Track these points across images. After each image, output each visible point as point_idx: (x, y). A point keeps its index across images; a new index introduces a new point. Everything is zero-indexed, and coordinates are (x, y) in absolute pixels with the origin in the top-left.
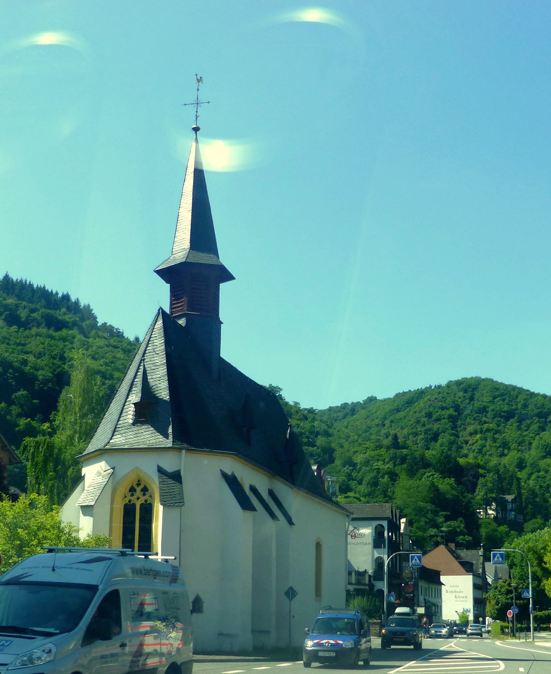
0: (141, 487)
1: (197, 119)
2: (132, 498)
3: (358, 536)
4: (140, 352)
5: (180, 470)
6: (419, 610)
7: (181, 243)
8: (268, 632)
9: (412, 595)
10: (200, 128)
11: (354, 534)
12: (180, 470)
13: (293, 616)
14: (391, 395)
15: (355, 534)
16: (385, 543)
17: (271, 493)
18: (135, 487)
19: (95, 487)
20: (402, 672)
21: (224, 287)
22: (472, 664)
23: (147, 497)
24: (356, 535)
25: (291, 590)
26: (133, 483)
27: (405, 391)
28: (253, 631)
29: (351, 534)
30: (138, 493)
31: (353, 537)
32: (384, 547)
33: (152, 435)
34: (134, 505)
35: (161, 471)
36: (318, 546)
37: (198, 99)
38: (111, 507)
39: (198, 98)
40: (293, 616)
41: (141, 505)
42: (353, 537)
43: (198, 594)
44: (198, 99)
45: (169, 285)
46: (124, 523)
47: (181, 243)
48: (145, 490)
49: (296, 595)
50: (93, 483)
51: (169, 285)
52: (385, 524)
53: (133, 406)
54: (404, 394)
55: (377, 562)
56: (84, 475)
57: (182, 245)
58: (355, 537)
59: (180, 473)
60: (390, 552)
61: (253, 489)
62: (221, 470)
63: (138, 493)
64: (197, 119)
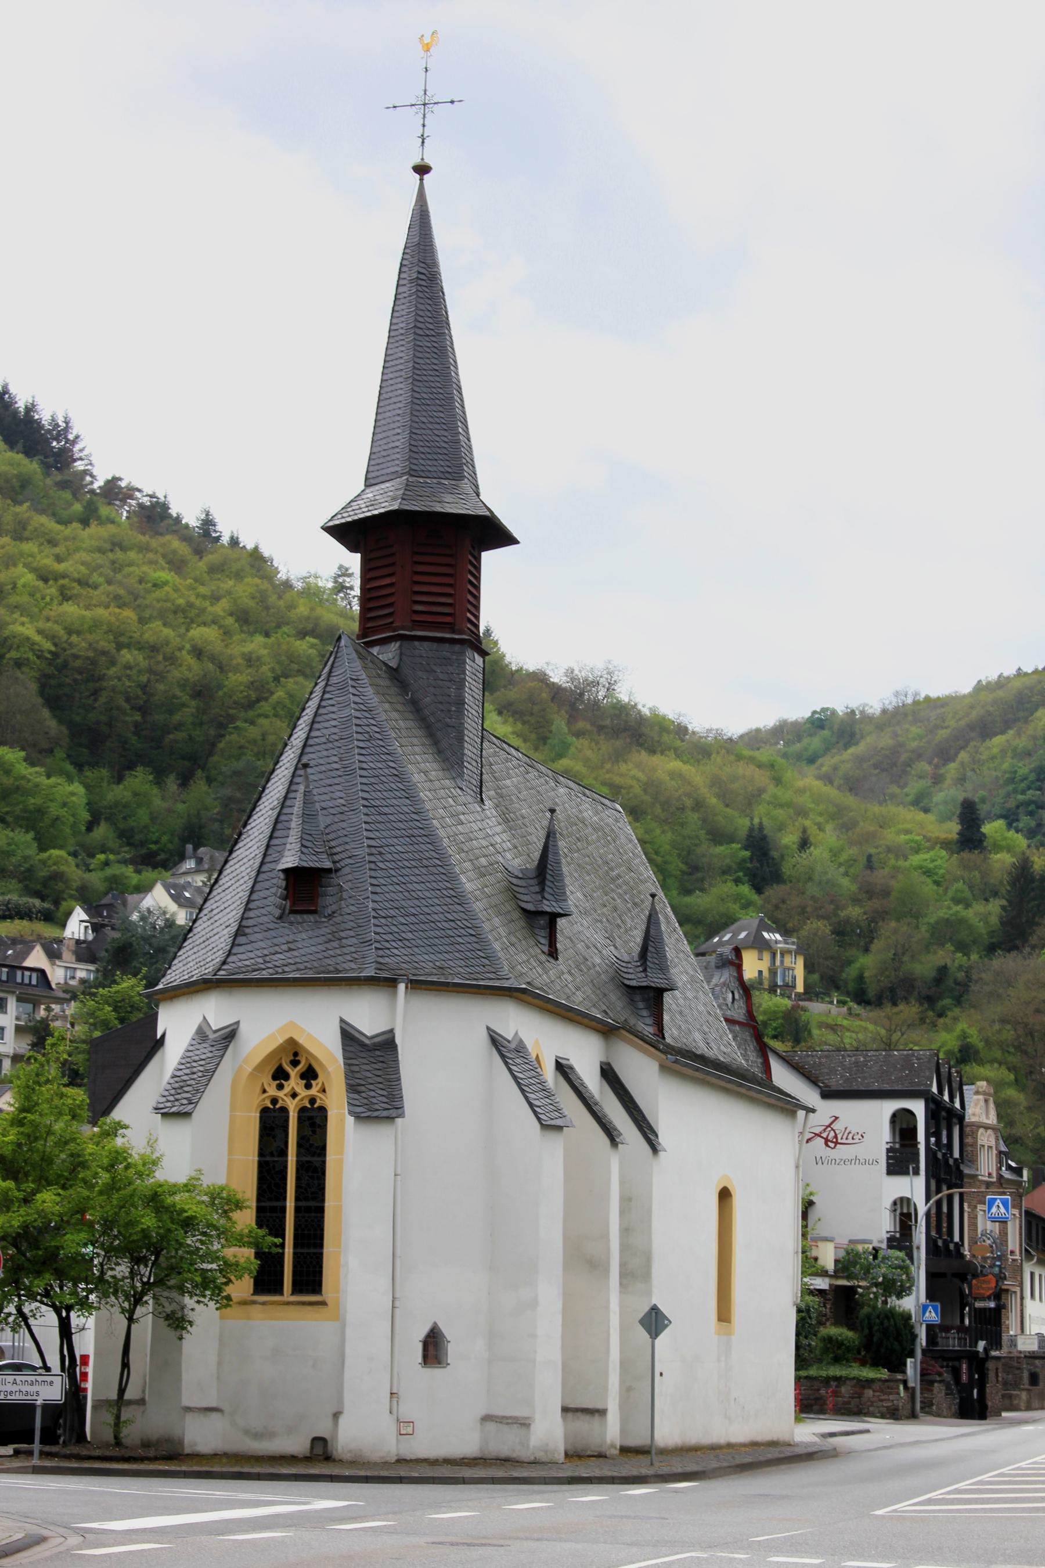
0: (301, 1067)
1: (423, 142)
2: (281, 1094)
3: (844, 1141)
4: (294, 743)
5: (391, 1031)
6: (1024, 1343)
7: (388, 459)
8: (602, 1412)
9: (992, 1305)
10: (432, 166)
11: (832, 1134)
12: (391, 1031)
13: (661, 1374)
14: (966, 688)
15: (836, 1137)
16: (918, 1162)
17: (608, 1074)
18: (288, 1068)
19: (195, 1070)
20: (903, 1512)
21: (491, 560)
22: (1016, 1498)
23: (314, 1091)
24: (839, 1137)
25: (654, 1314)
26: (14, 637)
27: (1005, 674)
28: (565, 1410)
29: (824, 1135)
30: (294, 1083)
31: (830, 1144)
32: (916, 1172)
33: (327, 945)
34: (284, 1110)
35: (349, 1036)
36: (725, 1195)
37: (424, 115)
38: (231, 1116)
39: (425, 91)
40: (661, 1374)
41: (302, 1110)
42: (830, 1144)
43: (435, 1323)
44: (424, 115)
45: (359, 555)
46: (261, 1153)
47: (388, 459)
48: (310, 1075)
49: (667, 1326)
50: (188, 1060)
51: (359, 555)
52: (918, 1108)
53: (282, 875)
54: (1002, 682)
55: (898, 1212)
56: (163, 1036)
57: (389, 464)
58: (836, 1143)
59: (394, 1037)
60: (933, 1187)
61: (563, 1069)
62: (488, 1028)
63: (294, 1083)
64: (423, 142)
